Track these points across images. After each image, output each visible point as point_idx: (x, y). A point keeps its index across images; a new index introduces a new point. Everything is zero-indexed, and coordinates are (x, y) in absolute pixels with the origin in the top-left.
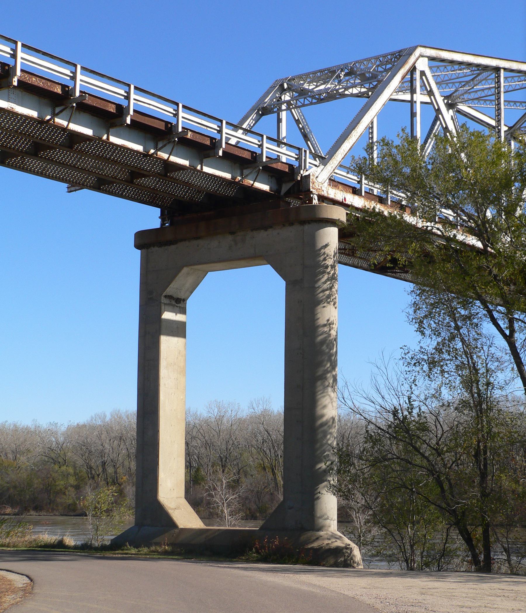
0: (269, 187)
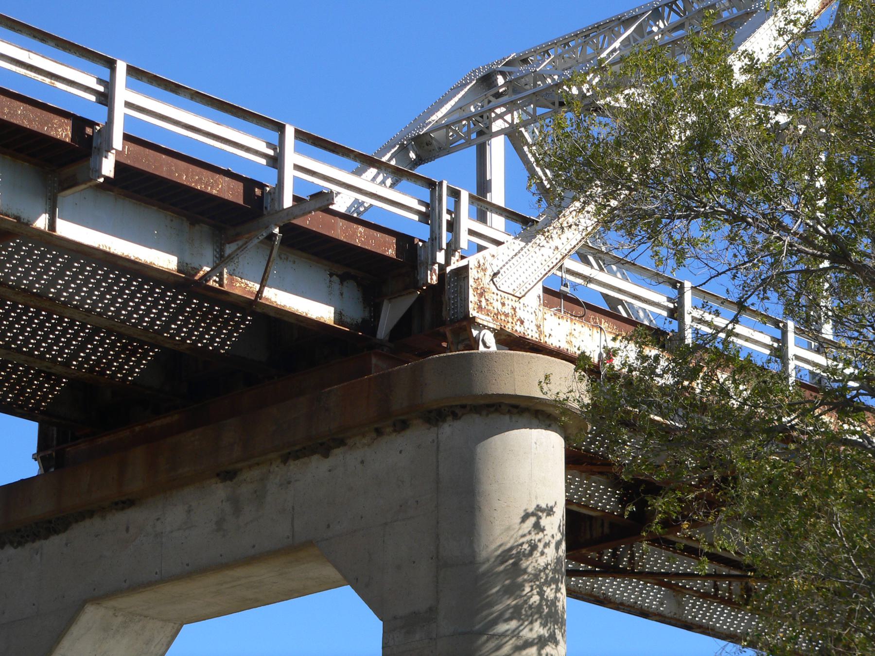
0: (332, 309)
